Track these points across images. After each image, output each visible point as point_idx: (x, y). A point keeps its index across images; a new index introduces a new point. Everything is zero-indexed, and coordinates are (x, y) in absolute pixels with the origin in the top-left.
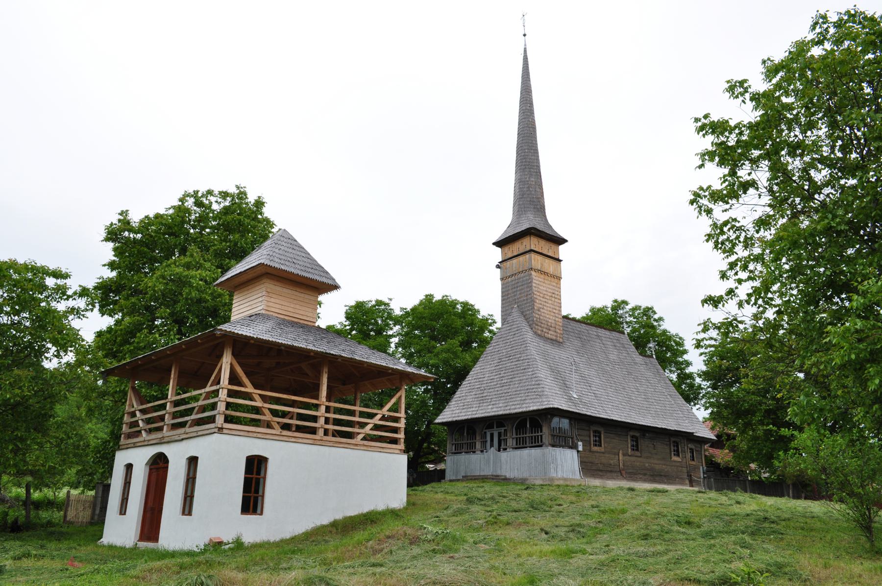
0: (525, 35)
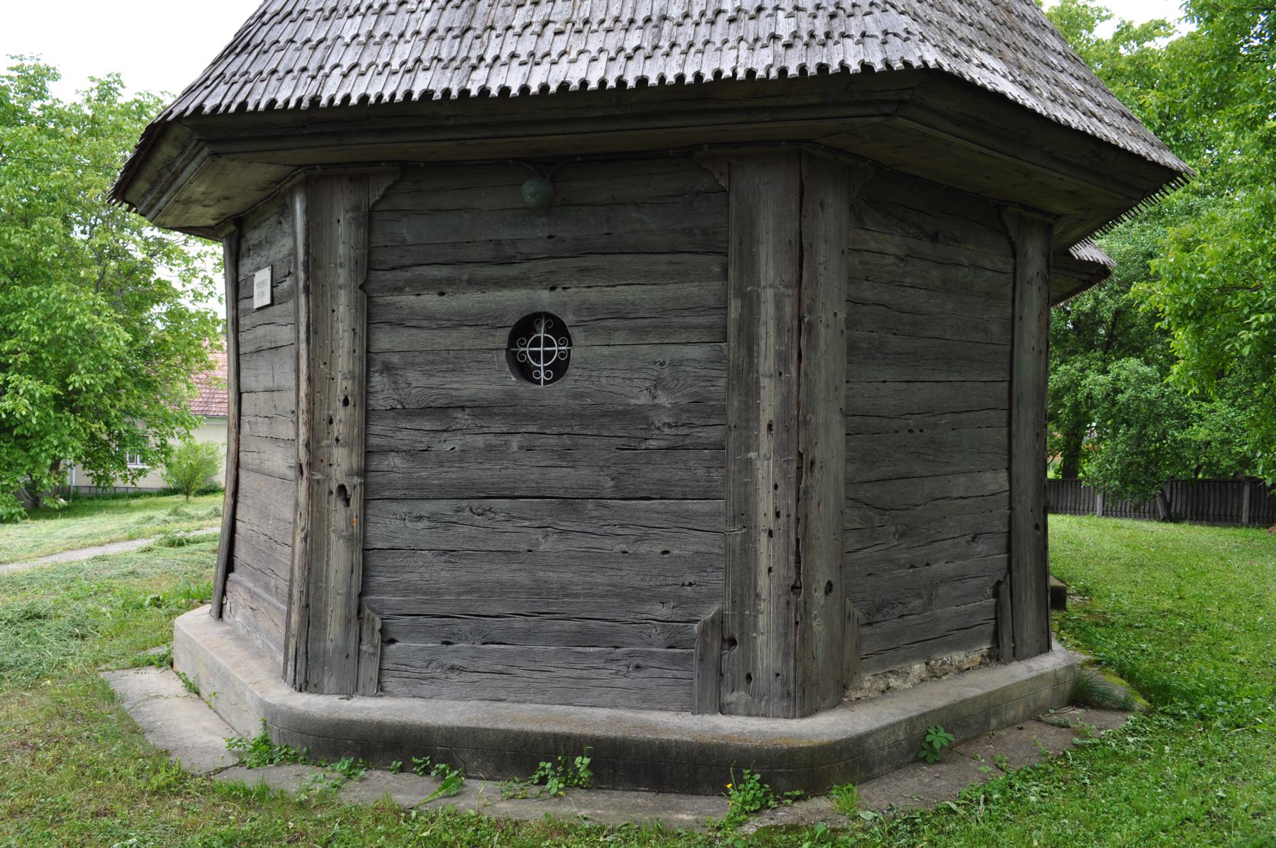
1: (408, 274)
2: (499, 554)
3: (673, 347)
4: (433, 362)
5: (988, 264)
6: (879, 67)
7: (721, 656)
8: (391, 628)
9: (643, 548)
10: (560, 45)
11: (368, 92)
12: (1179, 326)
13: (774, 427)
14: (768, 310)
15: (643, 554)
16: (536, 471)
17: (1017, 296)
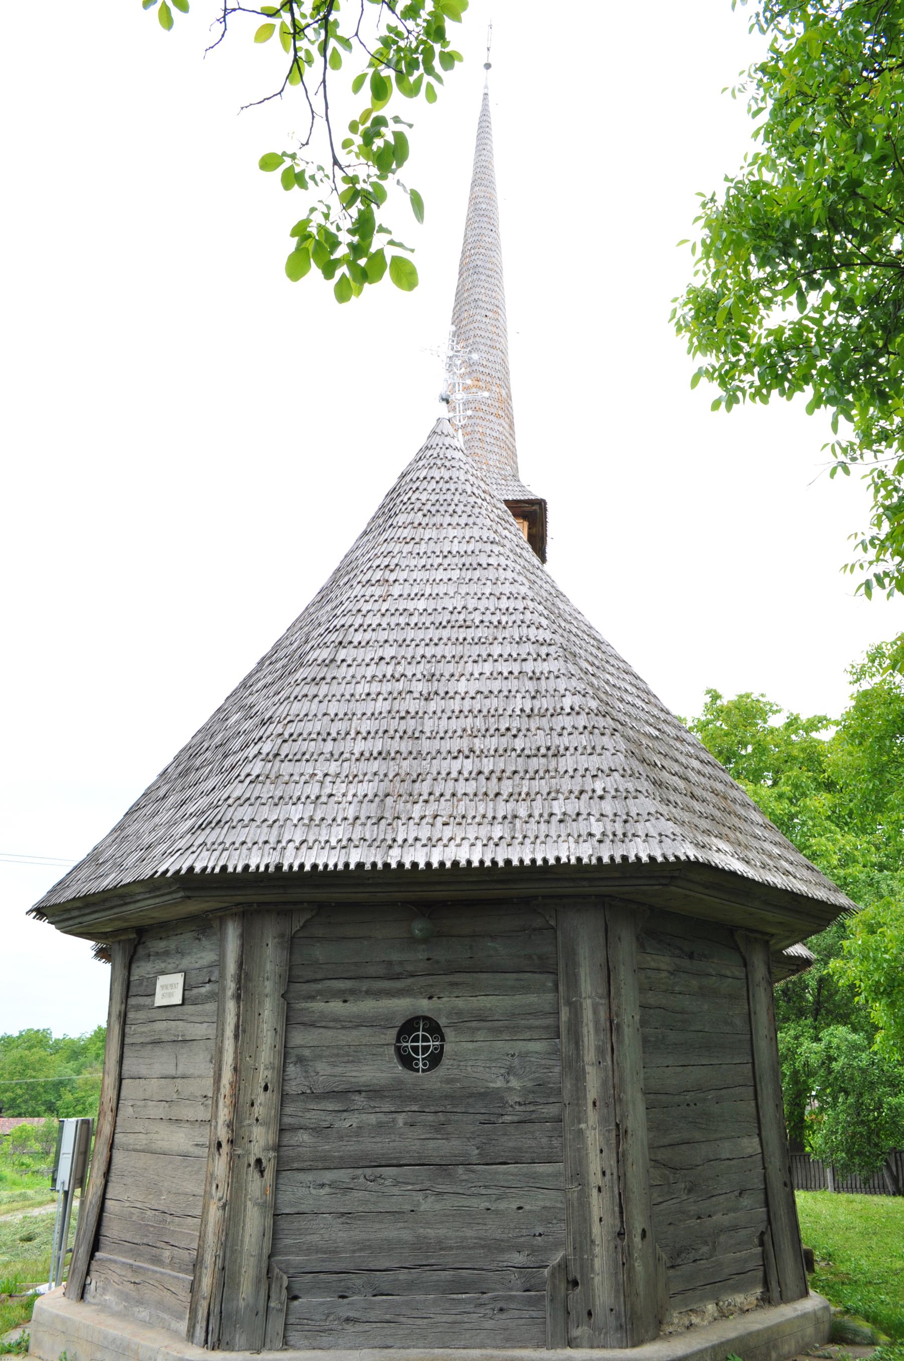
1: (319, 986)
2: (387, 1215)
3: (520, 1043)
4: (337, 1055)
5: (728, 973)
6: (660, 859)
7: (567, 1296)
8: (295, 1286)
9: (502, 1205)
10: (448, 832)
11: (317, 862)
12: (874, 1000)
13: (597, 1104)
14: (588, 1015)
15: (502, 1210)
16: (417, 1142)
17: (751, 996)
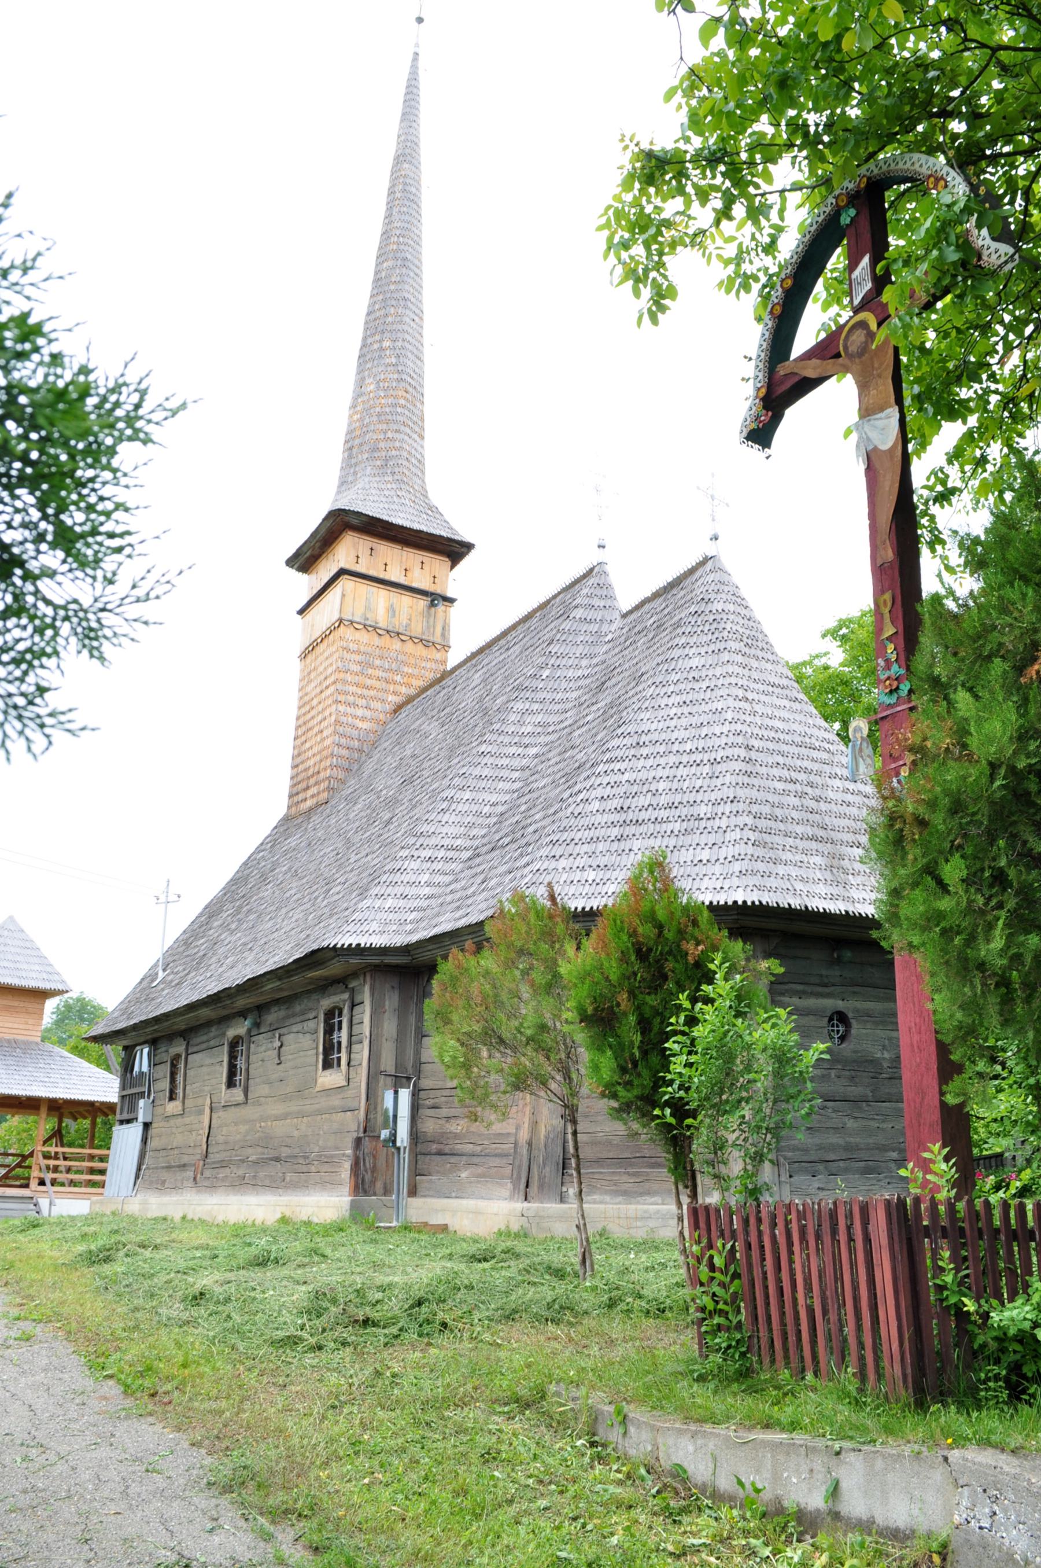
0: (420, 20)
1: (786, 987)
